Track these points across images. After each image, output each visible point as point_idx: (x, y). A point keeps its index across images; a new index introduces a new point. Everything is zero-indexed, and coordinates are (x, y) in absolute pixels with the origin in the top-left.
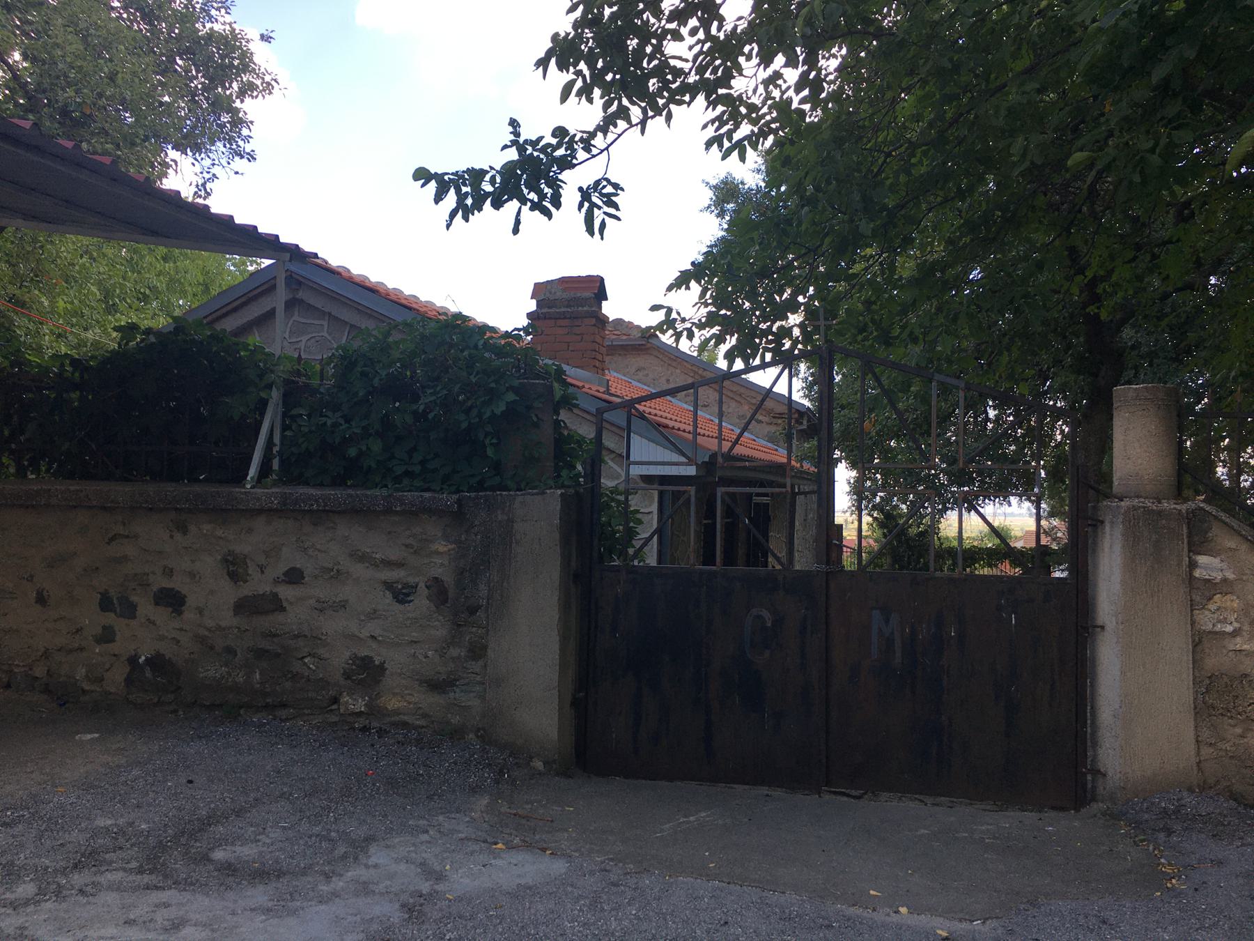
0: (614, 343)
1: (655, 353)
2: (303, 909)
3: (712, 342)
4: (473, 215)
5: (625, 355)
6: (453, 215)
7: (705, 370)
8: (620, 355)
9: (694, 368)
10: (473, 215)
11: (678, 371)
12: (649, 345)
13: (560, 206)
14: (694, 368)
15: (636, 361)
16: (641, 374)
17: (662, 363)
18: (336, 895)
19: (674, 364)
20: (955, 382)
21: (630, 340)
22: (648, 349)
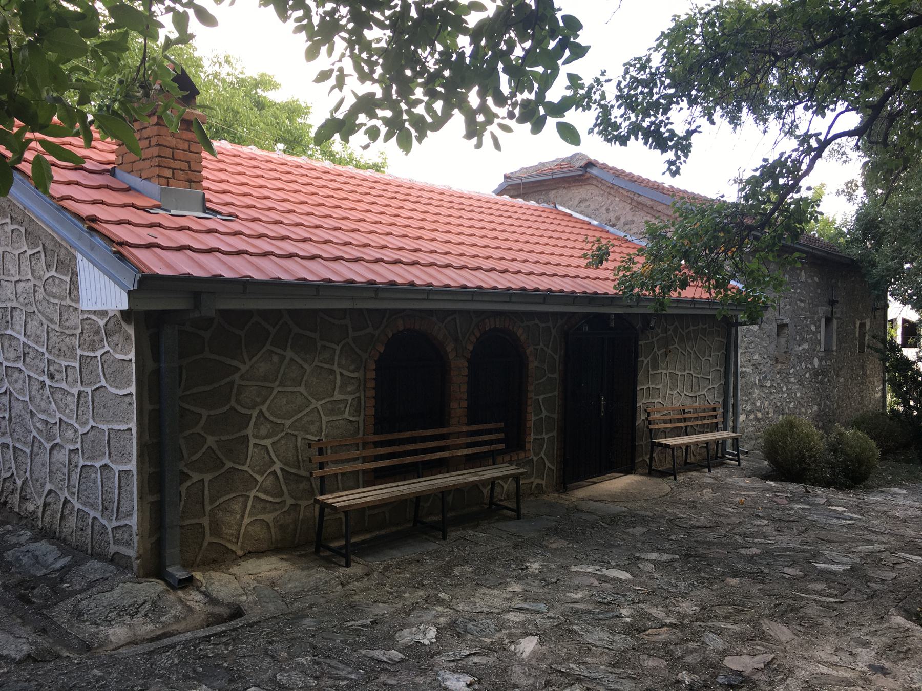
0: (554, 176)
1: (595, 182)
2: (634, 649)
3: (804, 167)
4: (576, 109)
5: (569, 187)
6: (333, 88)
7: (640, 195)
8: (564, 188)
9: (629, 194)
10: (576, 109)
11: (617, 199)
12: (588, 175)
13: (577, 75)
14: (629, 194)
15: (579, 193)
16: (583, 205)
17: (602, 192)
18: (776, 634)
19: (612, 192)
20: (289, 431)
21: (572, 171)
22: (588, 179)
